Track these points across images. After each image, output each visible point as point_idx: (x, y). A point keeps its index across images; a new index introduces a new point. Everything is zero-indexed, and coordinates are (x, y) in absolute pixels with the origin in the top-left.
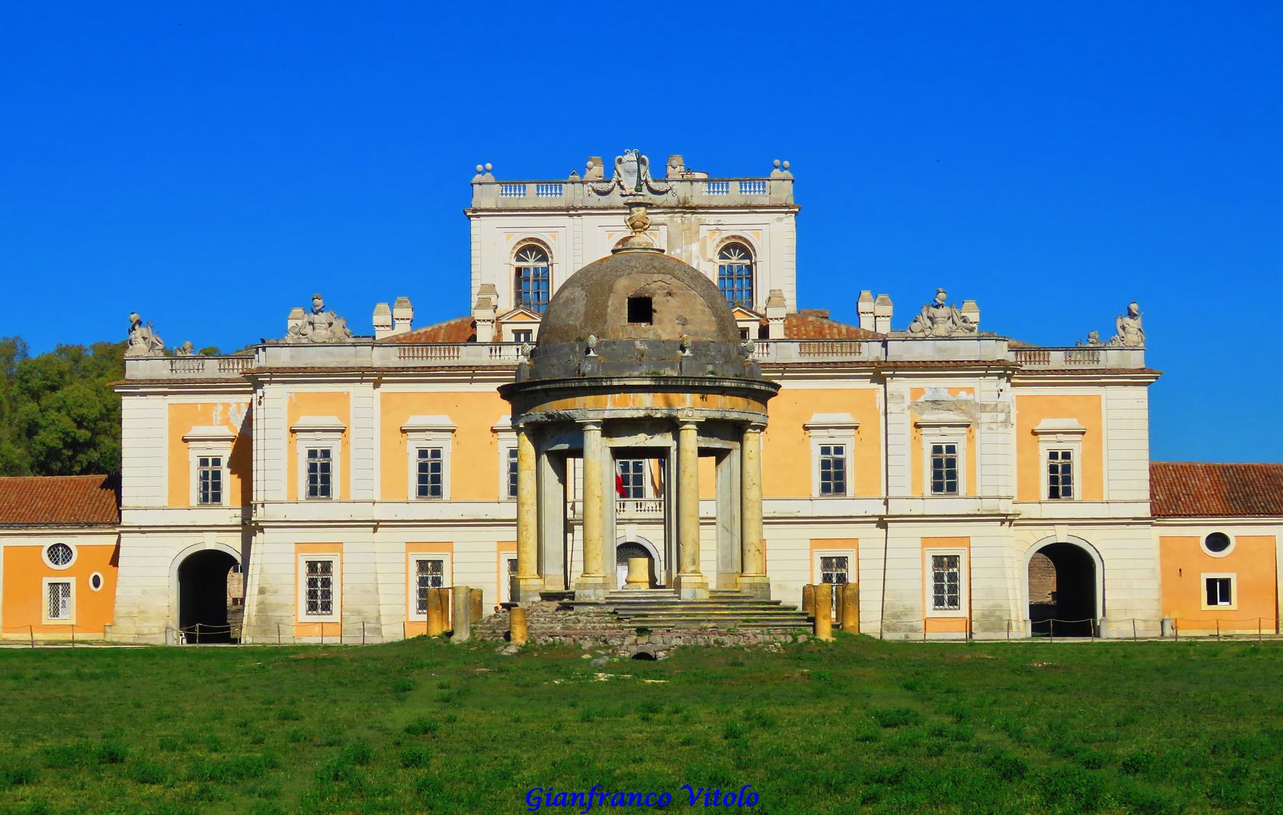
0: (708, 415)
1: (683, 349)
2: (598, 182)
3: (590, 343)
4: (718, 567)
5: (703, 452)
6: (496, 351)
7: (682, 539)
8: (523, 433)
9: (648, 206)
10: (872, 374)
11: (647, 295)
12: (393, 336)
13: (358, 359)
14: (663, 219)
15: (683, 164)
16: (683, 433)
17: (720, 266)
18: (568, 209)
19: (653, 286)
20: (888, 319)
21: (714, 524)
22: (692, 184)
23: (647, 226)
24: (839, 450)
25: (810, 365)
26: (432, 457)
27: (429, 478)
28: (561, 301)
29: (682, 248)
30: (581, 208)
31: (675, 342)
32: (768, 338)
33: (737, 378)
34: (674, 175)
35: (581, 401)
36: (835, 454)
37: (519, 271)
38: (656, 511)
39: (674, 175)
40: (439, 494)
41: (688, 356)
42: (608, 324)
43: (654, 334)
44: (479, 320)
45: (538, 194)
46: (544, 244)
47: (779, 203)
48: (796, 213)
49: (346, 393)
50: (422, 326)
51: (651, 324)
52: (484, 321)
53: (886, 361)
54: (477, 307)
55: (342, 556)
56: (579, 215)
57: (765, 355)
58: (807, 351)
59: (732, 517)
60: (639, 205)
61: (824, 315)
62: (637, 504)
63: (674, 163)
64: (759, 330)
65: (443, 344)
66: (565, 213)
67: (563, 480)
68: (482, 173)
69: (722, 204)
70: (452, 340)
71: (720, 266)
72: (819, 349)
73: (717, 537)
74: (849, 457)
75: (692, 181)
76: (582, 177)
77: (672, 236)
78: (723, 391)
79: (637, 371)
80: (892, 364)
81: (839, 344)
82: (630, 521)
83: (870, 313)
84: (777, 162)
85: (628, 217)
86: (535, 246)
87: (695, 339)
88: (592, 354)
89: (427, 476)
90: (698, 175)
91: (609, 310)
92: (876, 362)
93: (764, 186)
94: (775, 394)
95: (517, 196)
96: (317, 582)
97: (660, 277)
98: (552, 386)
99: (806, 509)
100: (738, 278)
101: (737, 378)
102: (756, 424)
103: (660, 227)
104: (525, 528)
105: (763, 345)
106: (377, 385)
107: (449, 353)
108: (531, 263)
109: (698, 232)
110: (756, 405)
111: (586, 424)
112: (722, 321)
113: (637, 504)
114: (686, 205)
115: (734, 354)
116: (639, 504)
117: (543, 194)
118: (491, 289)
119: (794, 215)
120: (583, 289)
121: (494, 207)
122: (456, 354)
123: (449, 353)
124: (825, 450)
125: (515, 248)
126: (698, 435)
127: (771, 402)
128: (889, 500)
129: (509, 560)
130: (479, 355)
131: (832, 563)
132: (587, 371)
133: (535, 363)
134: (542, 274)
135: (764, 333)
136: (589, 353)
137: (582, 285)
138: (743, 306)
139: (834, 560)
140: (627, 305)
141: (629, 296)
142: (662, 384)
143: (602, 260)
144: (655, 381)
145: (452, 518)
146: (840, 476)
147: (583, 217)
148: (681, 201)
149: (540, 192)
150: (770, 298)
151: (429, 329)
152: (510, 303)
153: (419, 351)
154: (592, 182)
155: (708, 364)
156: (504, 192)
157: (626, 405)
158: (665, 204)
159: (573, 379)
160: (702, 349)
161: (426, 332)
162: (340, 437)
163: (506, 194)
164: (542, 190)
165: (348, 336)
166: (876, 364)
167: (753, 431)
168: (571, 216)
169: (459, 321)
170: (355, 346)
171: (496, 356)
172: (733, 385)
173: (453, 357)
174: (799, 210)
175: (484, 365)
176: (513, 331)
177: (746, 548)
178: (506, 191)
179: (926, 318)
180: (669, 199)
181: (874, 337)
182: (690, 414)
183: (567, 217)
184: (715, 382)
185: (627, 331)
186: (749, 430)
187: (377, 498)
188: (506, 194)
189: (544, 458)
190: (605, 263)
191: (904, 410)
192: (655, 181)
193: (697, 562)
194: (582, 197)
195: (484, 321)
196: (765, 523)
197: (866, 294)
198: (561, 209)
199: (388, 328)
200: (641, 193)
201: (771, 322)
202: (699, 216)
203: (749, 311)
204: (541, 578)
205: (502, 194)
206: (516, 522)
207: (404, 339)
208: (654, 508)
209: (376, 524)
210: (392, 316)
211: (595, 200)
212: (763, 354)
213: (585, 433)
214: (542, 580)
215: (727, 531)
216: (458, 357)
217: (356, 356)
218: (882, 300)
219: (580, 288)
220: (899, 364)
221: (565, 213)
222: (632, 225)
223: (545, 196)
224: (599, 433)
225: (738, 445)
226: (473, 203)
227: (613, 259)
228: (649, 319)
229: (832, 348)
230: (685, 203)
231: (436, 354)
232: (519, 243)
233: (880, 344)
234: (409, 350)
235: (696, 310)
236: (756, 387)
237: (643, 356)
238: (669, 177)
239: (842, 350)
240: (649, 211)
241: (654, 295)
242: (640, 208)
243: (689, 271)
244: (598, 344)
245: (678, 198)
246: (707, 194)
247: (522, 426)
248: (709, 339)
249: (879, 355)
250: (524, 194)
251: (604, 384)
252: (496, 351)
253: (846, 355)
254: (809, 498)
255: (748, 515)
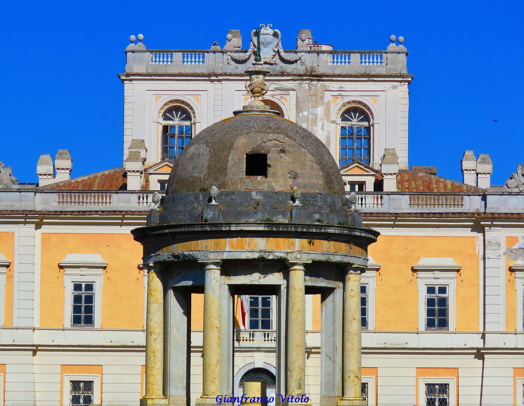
0: (315, 257)
1: (293, 199)
2: (236, 52)
3: (212, 192)
4: (321, 391)
5: (309, 290)
6: (143, 198)
7: (290, 367)
8: (153, 271)
9: (265, 74)
10: (472, 224)
11: (263, 152)
12: (54, 184)
13: (22, 204)
14: (292, 85)
15: (311, 38)
16: (292, 273)
17: (342, 127)
18: (209, 75)
19: (269, 144)
20: (488, 176)
21: (319, 353)
22: (318, 55)
23: (264, 92)
24: (443, 290)
25: (419, 215)
26: (440, 292)
27: (83, 309)
28: (188, 156)
29: (309, 111)
30: (221, 75)
31: (286, 194)
32: (383, 191)
33: (341, 226)
34: (303, 46)
35: (202, 244)
36: (439, 293)
37: (165, 129)
38: (250, 340)
39: (303, 46)
40: (92, 323)
41: (297, 206)
42: (228, 176)
43: (268, 186)
44: (130, 171)
45: (183, 62)
46: (188, 105)
47: (394, 73)
48: (409, 82)
49: (10, 233)
50: (79, 176)
51: (266, 177)
52: (133, 171)
53: (485, 213)
54: (128, 160)
55: (5, 377)
56: (220, 81)
57: (379, 206)
58: (416, 203)
59: (335, 348)
60: (258, 73)
61: (433, 172)
62: (265, 334)
63: (303, 36)
64: (374, 183)
65: (98, 192)
66: (207, 78)
67: (188, 312)
68: (135, 42)
69: (344, 73)
70: (105, 188)
71: (342, 127)
72: (426, 201)
73: (322, 365)
74: (451, 296)
75: (318, 53)
76: (222, 47)
77: (300, 100)
78: (328, 237)
79: (252, 218)
80: (490, 216)
81: (436, 197)
82: (258, 349)
83: (473, 170)
84: (393, 37)
85: (248, 83)
86: (180, 107)
87: (304, 191)
88: (214, 202)
89: (81, 307)
90: (325, 48)
91: (229, 164)
92: (477, 213)
93: (381, 58)
94: (375, 241)
95: (165, 63)
96: (80, 398)
97: (275, 136)
98: (178, 230)
99: (413, 341)
100: (357, 138)
101: (341, 226)
102: (357, 266)
103: (290, 92)
104: (152, 354)
105: (377, 197)
106: (38, 226)
107: (102, 199)
108: (176, 122)
109: (322, 97)
110: (357, 250)
111: (207, 264)
112: (329, 175)
113: (265, 334)
114: (313, 74)
115: (339, 205)
116: (266, 335)
117: (187, 62)
118: (140, 144)
119: (407, 83)
120: (207, 146)
121: (145, 72)
122: (108, 201)
123: (102, 199)
124: (431, 290)
125: (162, 108)
126: (306, 275)
127: (370, 247)
128: (486, 335)
129: (71, 381)
130: (129, 201)
131: (435, 389)
132: (209, 218)
133: (164, 210)
134: (186, 132)
135: (379, 186)
136: (211, 202)
137: (206, 142)
138: (362, 163)
139: (437, 387)
140: (245, 160)
141: (247, 152)
142: (274, 229)
143: (224, 121)
144: (269, 227)
145: (102, 344)
146: (444, 312)
147: (223, 82)
148: (309, 70)
149: (186, 60)
150: (384, 155)
151: (86, 178)
152: (158, 156)
153: (76, 197)
154: (231, 52)
155: (315, 213)
156: (154, 59)
157: (243, 248)
158: (295, 72)
159: (196, 224)
160: (311, 199)
161: (83, 181)
162: (102, 273)
163: (156, 61)
164: (187, 58)
165: (14, 183)
166: (476, 215)
167: (354, 272)
168: (212, 81)
169: (112, 171)
170: (20, 192)
171: (143, 203)
172: (337, 231)
173: (106, 203)
174: (412, 79)
175: (133, 210)
176: (159, 181)
177: (346, 378)
178: (156, 58)
179: (520, 176)
180: (299, 68)
181: (475, 191)
182: (298, 256)
183: (209, 82)
184: (321, 229)
185: (245, 183)
186: (351, 271)
187: (37, 325)
188: (156, 61)
189: (171, 293)
190: (226, 124)
191: (500, 256)
192: (286, 52)
193: (302, 387)
194: (222, 65)
195: (133, 171)
196: (363, 353)
197: (469, 153)
198: (204, 75)
199: (50, 177)
200: (260, 63)
201: (385, 177)
202: (324, 83)
203: (366, 167)
204: (166, 398)
205: (153, 61)
206: (145, 349)
207: (64, 186)
208: (248, 338)
209: (35, 348)
210: (54, 166)
211: (233, 67)
212: (377, 204)
213: (207, 272)
214: (167, 400)
215: (330, 360)
216: (110, 203)
217: (21, 201)
218: (482, 159)
219: (205, 145)
220: (496, 215)
221: (207, 78)
222: (251, 91)
223: (189, 63)
224: (218, 272)
225: (341, 284)
226: (126, 68)
227: (234, 120)
228: (264, 173)
229: (438, 200)
230: (312, 72)
231: (91, 200)
232: (166, 104)
233: (480, 198)
234: (67, 196)
235: (306, 166)
236: (357, 234)
237: (258, 205)
238: (299, 49)
239: (446, 202)
240: (267, 78)
241: (269, 151)
242: (259, 76)
243: (301, 131)
244: (219, 194)
245: (306, 67)
246: (332, 64)
247: (151, 264)
248: (317, 191)
249: (479, 207)
250: (171, 62)
251: (224, 229)
252: (143, 198)
253: (414, 207)
254: (415, 331)
255: (348, 345)
